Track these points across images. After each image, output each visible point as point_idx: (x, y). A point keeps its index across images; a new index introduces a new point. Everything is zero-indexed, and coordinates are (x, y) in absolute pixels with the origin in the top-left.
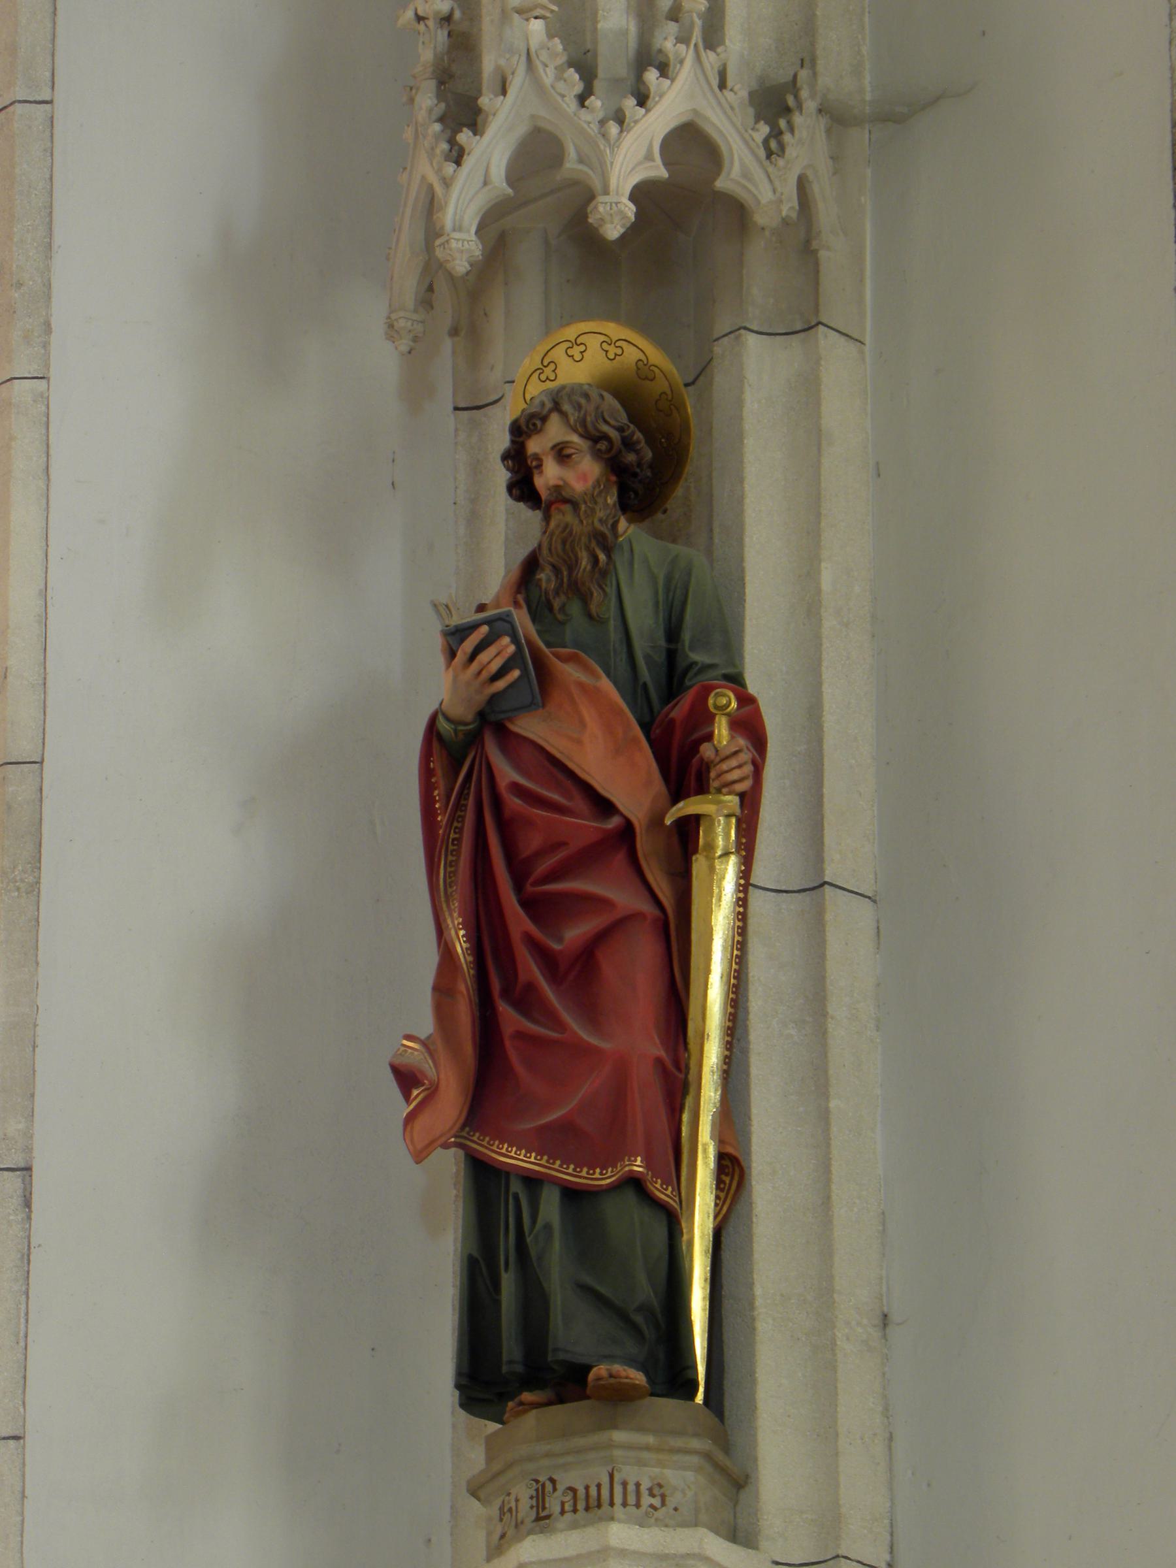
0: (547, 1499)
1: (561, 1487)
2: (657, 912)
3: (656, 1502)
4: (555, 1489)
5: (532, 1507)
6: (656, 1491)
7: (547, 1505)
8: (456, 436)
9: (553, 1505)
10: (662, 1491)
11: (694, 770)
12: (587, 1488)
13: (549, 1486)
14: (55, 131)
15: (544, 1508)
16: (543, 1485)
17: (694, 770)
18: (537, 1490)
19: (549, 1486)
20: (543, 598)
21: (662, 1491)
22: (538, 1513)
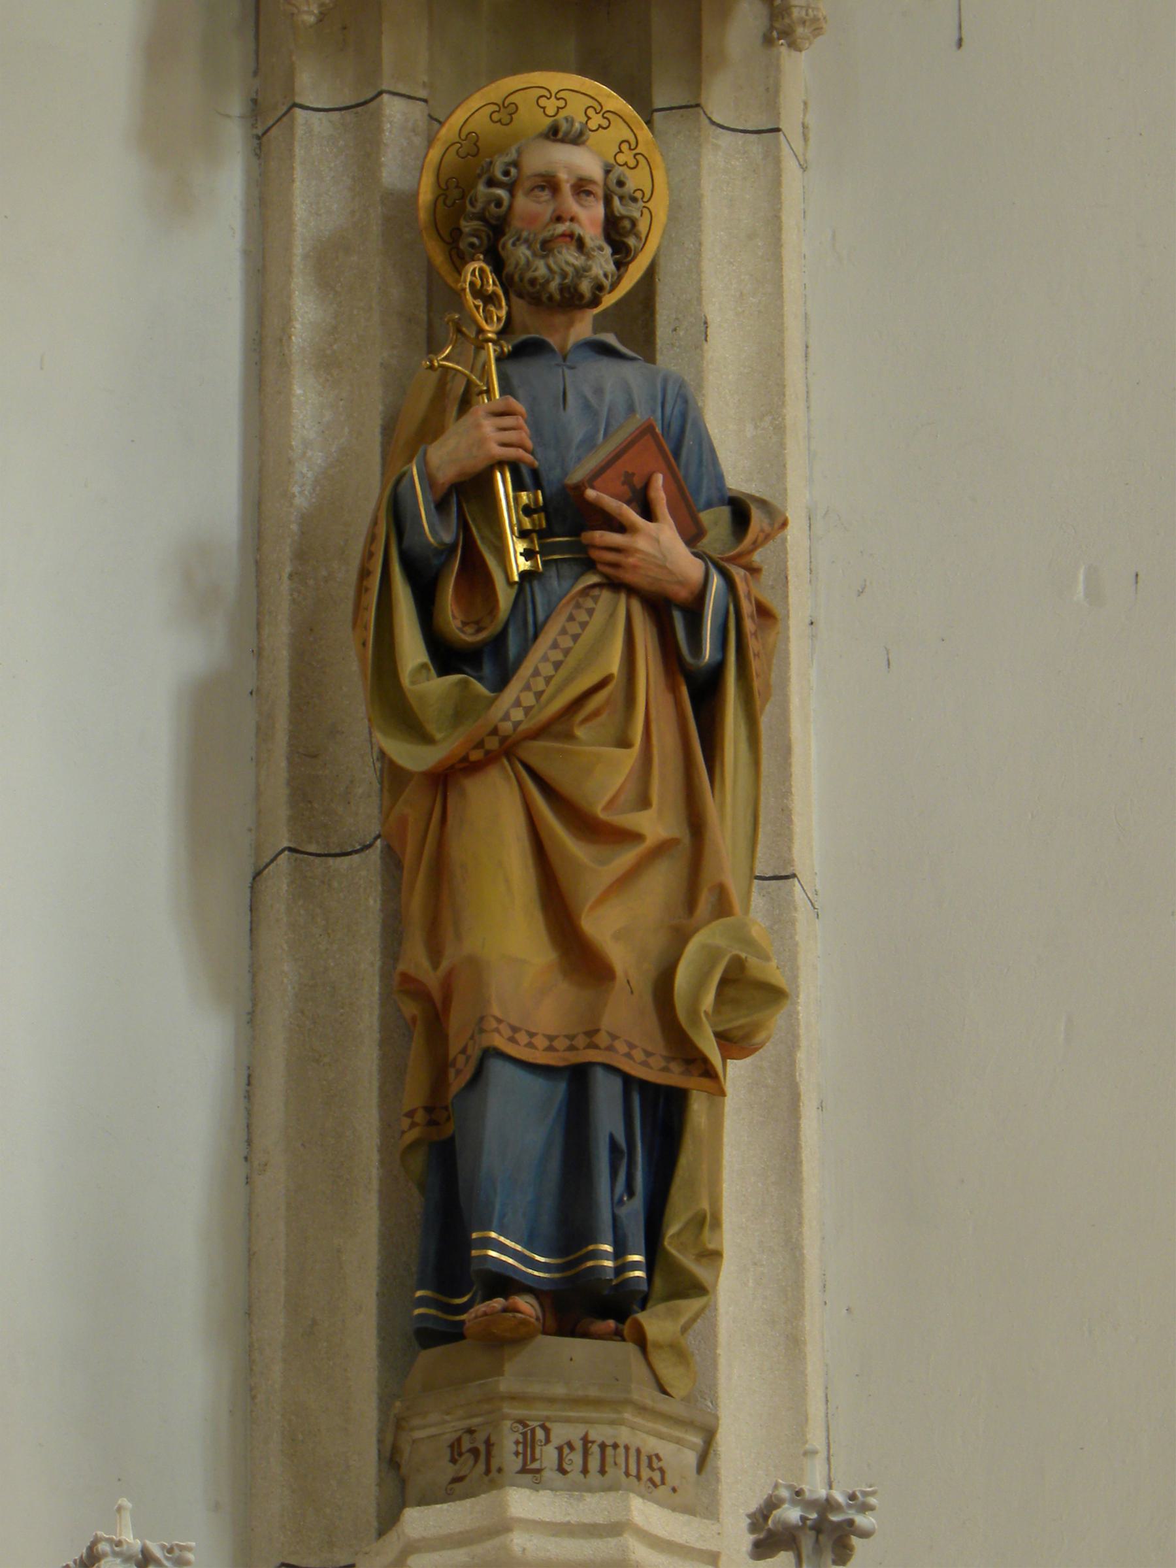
0: (537, 1451)
1: (556, 1441)
2: (286, 852)
3: (657, 1477)
4: (548, 1441)
5: (517, 1454)
6: (656, 1464)
7: (537, 1456)
8: (651, 1068)
9: (548, 1456)
10: (661, 1464)
11: (584, 1251)
12: (585, 1471)
13: (540, 1434)
14: (824, 1434)
15: (533, 1460)
16: (533, 1431)
17: (584, 1251)
18: (524, 1434)
19: (540, 1434)
20: (314, 84)
21: (661, 1464)
22: (525, 1463)
